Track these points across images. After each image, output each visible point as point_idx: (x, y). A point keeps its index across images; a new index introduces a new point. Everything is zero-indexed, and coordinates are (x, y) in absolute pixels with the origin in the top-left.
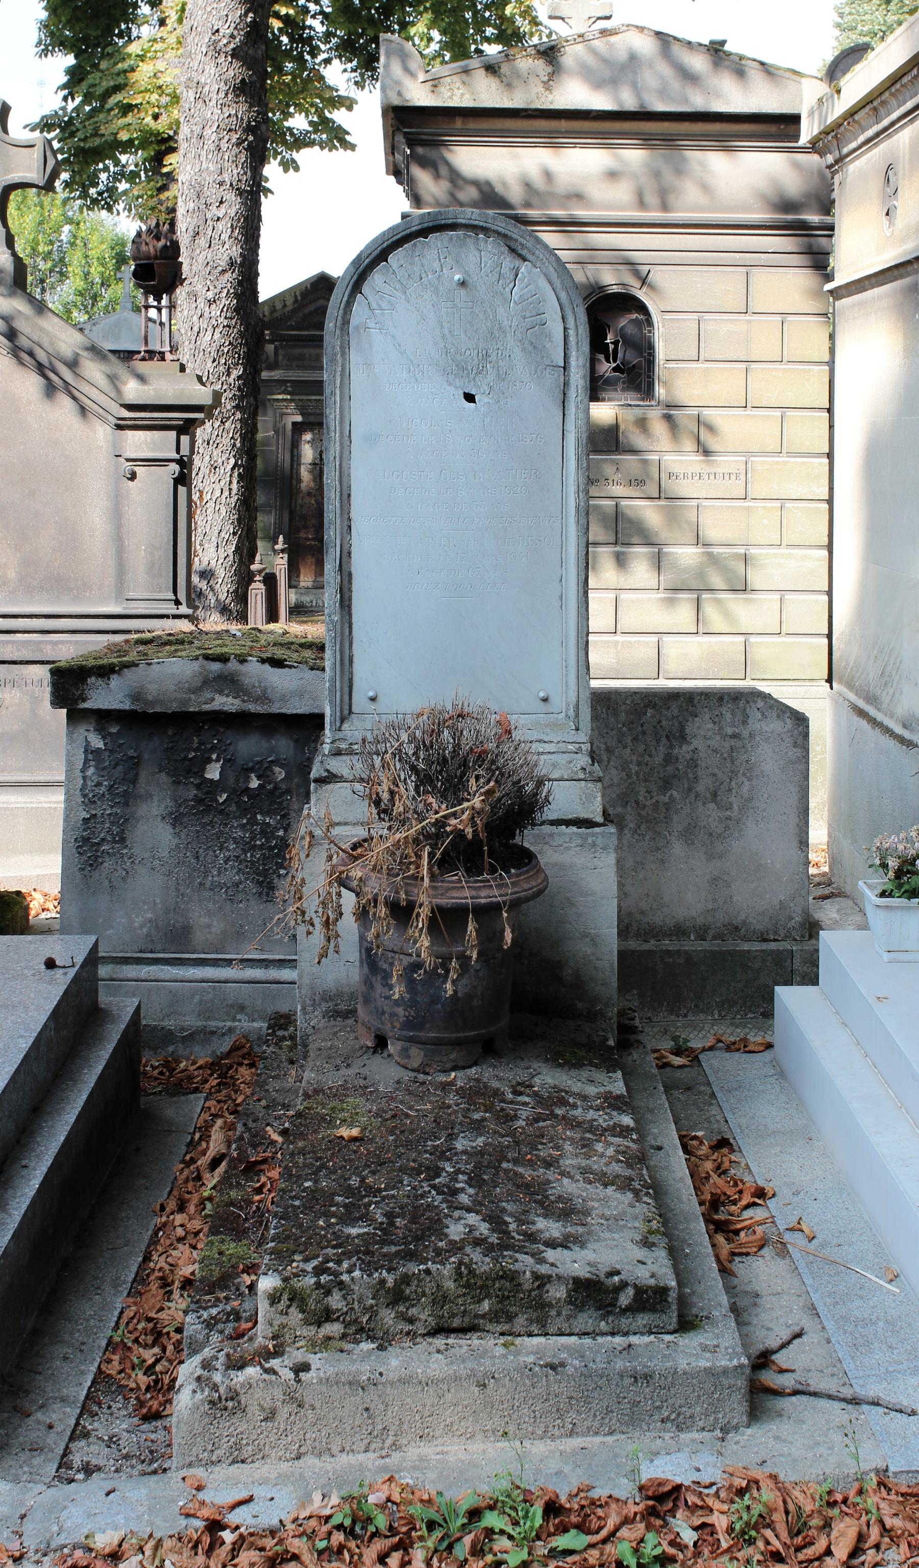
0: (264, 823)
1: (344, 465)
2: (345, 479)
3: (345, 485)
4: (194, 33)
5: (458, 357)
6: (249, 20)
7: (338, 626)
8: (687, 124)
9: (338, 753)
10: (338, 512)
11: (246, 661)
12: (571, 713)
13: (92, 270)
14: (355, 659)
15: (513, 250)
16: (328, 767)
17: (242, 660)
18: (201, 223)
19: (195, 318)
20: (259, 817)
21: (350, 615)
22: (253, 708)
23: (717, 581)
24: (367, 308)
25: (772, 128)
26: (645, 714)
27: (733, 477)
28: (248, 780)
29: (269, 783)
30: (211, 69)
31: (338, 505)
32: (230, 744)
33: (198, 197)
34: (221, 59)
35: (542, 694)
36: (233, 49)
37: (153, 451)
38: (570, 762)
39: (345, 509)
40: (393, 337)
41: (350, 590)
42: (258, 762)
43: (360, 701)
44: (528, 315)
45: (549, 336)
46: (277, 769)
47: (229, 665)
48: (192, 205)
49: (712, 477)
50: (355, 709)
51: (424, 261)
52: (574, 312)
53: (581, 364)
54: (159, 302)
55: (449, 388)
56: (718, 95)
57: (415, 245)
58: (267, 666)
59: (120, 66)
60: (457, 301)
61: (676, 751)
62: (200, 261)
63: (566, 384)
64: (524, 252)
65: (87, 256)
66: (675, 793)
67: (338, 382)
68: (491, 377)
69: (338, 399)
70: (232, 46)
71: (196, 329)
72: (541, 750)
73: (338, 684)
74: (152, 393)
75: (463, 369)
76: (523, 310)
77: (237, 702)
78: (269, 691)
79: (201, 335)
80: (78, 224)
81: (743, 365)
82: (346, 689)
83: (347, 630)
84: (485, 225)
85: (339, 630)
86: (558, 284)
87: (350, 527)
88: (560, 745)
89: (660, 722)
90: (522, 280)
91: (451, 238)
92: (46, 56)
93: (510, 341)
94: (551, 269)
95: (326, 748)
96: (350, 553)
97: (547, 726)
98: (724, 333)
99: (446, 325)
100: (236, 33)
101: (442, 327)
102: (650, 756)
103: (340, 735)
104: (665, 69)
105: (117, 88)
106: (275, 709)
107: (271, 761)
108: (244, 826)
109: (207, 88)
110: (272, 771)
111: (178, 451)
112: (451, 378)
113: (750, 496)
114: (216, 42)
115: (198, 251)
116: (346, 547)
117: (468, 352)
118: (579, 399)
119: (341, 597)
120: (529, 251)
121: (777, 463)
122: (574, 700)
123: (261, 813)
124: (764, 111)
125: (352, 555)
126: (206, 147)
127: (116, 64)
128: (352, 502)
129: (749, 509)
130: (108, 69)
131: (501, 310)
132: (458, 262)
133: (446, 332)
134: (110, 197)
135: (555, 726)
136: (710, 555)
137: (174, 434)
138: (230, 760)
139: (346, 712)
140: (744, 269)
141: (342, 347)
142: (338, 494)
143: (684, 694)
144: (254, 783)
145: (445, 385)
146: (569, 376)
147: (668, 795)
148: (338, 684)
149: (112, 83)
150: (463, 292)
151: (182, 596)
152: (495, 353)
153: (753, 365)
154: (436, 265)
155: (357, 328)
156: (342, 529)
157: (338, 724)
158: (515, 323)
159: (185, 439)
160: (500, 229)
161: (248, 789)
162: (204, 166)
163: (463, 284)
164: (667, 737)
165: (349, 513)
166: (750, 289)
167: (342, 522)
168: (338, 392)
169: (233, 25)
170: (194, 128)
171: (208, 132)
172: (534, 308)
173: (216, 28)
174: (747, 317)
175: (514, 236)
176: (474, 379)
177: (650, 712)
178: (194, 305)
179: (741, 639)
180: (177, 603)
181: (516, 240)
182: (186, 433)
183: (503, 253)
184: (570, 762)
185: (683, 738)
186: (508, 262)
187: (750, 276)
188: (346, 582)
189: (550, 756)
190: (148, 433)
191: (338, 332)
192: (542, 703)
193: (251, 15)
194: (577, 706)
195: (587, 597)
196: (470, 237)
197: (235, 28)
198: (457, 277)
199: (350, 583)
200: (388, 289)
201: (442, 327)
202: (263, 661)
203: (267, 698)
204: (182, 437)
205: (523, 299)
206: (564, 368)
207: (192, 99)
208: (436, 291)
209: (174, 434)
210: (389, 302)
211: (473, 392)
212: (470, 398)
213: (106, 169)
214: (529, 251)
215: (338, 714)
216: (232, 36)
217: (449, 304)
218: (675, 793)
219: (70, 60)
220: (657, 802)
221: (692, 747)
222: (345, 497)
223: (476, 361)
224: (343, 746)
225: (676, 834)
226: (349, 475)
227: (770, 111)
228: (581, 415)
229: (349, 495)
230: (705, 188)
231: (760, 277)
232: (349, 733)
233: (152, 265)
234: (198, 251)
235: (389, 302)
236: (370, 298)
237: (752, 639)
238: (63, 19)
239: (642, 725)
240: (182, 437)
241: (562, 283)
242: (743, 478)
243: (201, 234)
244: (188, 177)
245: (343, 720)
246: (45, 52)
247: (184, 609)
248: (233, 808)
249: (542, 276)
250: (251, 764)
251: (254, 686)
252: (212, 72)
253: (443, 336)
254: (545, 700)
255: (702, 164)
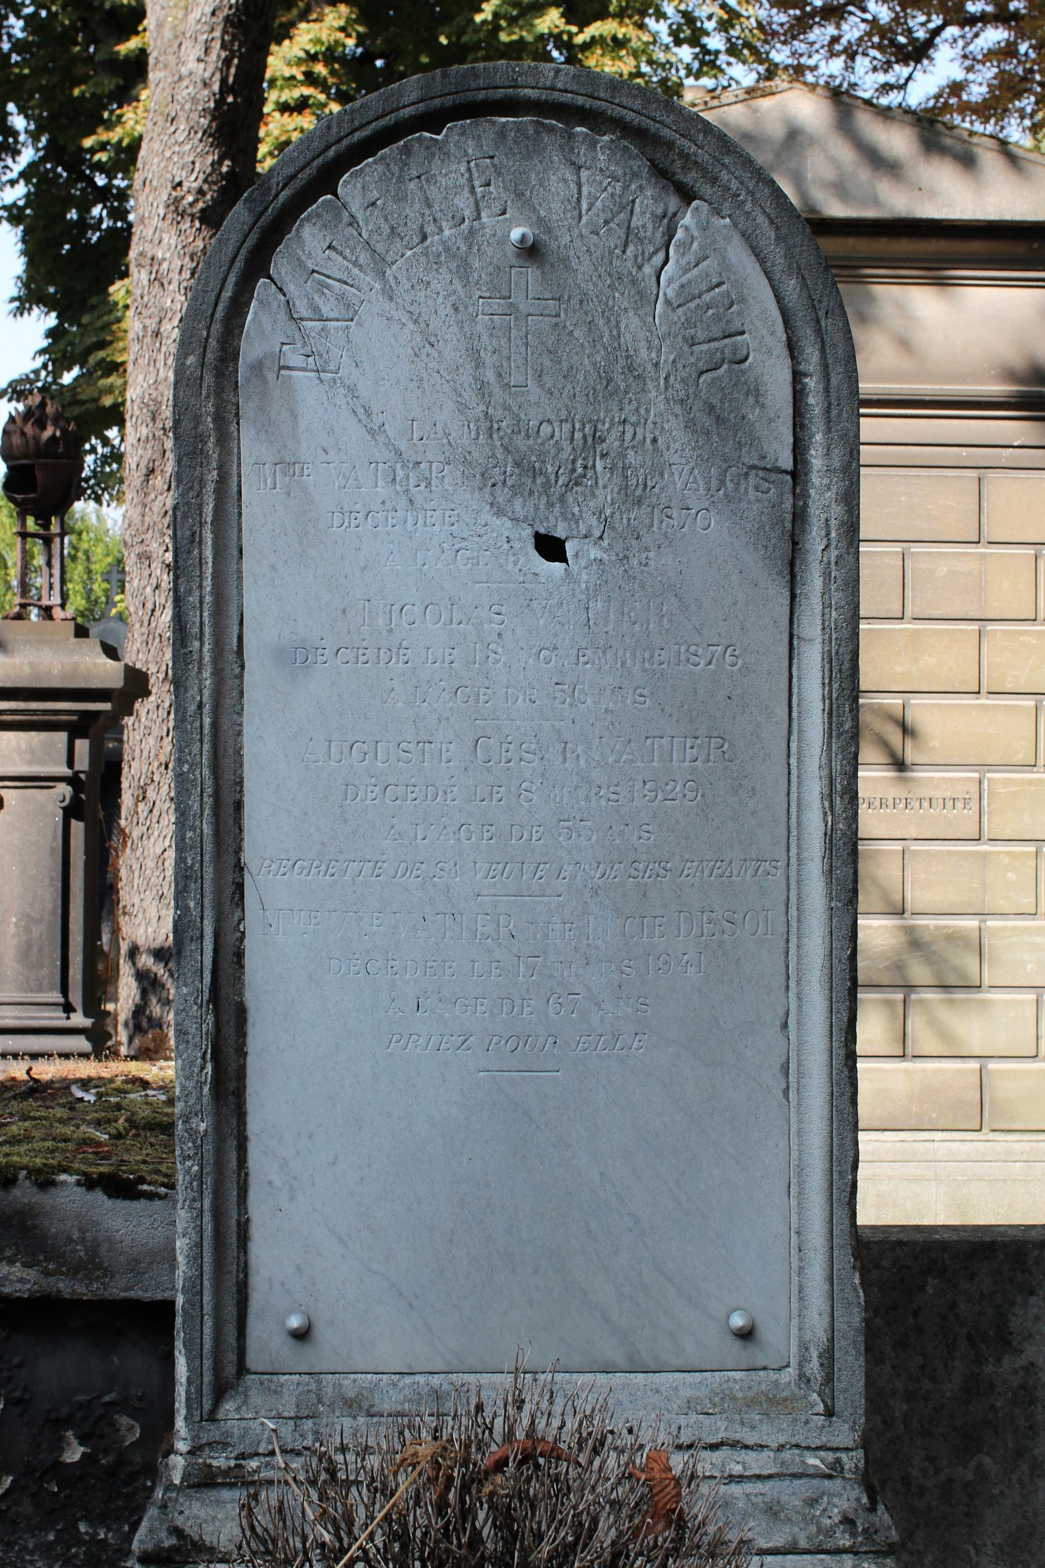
0: (94, 1540)
1: (225, 725)
2: (227, 762)
3: (228, 776)
4: (147, 189)
5: (519, 441)
6: (224, 169)
7: (208, 1147)
8: (884, 240)
9: (204, 1481)
10: (208, 847)
11: (53, 1183)
12: (814, 1366)
13: (96, 587)
14: (256, 1232)
15: (661, 173)
16: (179, 1521)
17: (44, 1180)
18: (157, 455)
19: (149, 590)
20: (83, 1528)
21: (241, 1116)
22: (65, 1287)
23: (919, 973)
24: (283, 316)
25: (1019, 248)
26: (922, 1288)
27: (959, 805)
28: (59, 1445)
29: (106, 1452)
30: (170, 238)
31: (207, 829)
32: (21, 1365)
33: (154, 419)
34: (186, 225)
35: (738, 1321)
36: (202, 211)
37: (30, 762)
38: (813, 1502)
39: (229, 840)
40: (352, 390)
41: (242, 1053)
42: (81, 1406)
43: (266, 1341)
44: (701, 335)
45: (756, 392)
46: (124, 1421)
47: (16, 1192)
48: (144, 431)
49: (926, 804)
50: (253, 1360)
51: (433, 192)
52: (819, 331)
53: (836, 464)
54: (46, 526)
55: (496, 522)
56: (932, 195)
57: (407, 150)
58: (99, 1197)
59: (105, 318)
60: (518, 297)
61: (989, 1369)
62: (155, 509)
63: (799, 517)
64: (690, 178)
65: (90, 571)
66: (987, 1461)
67: (209, 510)
68: (606, 495)
69: (208, 553)
70: (201, 205)
71: (149, 606)
72: (738, 1469)
73: (207, 1298)
74: (27, 670)
75: (535, 473)
76: (689, 324)
77: (31, 1274)
78: (103, 1250)
79: (157, 613)
80: (80, 534)
81: (974, 627)
82: (230, 1311)
83: (233, 1157)
84: (588, 103)
85: (209, 1156)
86: (778, 258)
87: (240, 887)
88: (787, 1455)
89: (953, 1305)
90: (685, 246)
91: (502, 133)
92: (22, 314)
93: (656, 401)
94: (761, 219)
95: (177, 1466)
96: (240, 955)
97: (751, 1403)
98: (943, 572)
99: (488, 359)
100: (206, 187)
101: (478, 364)
102: (933, 1379)
103: (213, 1432)
104: (844, 152)
105: (102, 345)
106: (117, 1290)
107: (112, 1403)
108: (51, 1546)
109: (165, 266)
110: (112, 1424)
111: (70, 763)
112: (502, 495)
113: (986, 834)
114: (177, 201)
115: (153, 496)
116: (231, 938)
117: (546, 430)
118: (834, 554)
119: (216, 1070)
120: (704, 171)
121: (1030, 782)
122: (822, 1336)
123: (88, 1518)
124: (1008, 217)
125: (249, 962)
126: (164, 349)
127: (100, 317)
128: (248, 823)
129: (985, 855)
130: (91, 323)
131: (631, 323)
132: (519, 195)
133: (490, 376)
134: (98, 484)
135: (772, 1404)
136: (909, 930)
137: (62, 737)
138: (19, 1401)
139: (230, 1370)
140: (974, 473)
141: (219, 419)
142: (208, 801)
143: (1005, 1244)
144: (74, 1453)
145: (486, 515)
146: (805, 496)
147: (973, 1464)
148: (207, 1298)
149: (94, 339)
150: (532, 273)
151: (76, 998)
152: (615, 433)
153: (991, 627)
154: (463, 203)
155: (258, 367)
156: (218, 893)
157: (207, 1405)
158: (667, 356)
159: (82, 746)
160: (630, 116)
161: (58, 1466)
162: (162, 375)
163: (531, 251)
164: (970, 1339)
165: (238, 850)
166: (985, 504)
167: (218, 874)
168: (208, 536)
169: (202, 176)
170: (148, 322)
171: (166, 327)
172: (717, 318)
173: (177, 180)
174: (980, 550)
175: (666, 133)
176: (562, 500)
177: (932, 1285)
178: (147, 572)
179: (974, 1065)
180: (68, 1008)
181: (670, 145)
182: (83, 735)
183: (635, 175)
184: (813, 1502)
185: (1004, 1341)
186: (649, 202)
187: (984, 484)
188: (229, 1031)
189: (759, 1487)
190: (22, 735)
191: (209, 379)
192: (738, 1343)
193: (227, 163)
194: (828, 1356)
195: (853, 1070)
196: (551, 130)
197: (205, 181)
198: (516, 234)
199: (241, 1033)
200: (337, 265)
201: (478, 364)
202: (89, 1183)
203: (99, 1267)
204: (78, 743)
205: (686, 295)
206: (794, 474)
207: (146, 283)
208: (464, 270)
209: (62, 737)
210: (341, 297)
211: (560, 533)
212: (551, 548)
213: (93, 450)
214: (704, 171)
215: (207, 1378)
216: (201, 192)
217: (496, 305)
218: (987, 1461)
219: (52, 320)
220: (950, 1480)
221: (1022, 1361)
222: (228, 810)
223: (566, 453)
224: (221, 1461)
225: (990, 1550)
226: (238, 753)
227: (1018, 218)
228: (837, 597)
229: (239, 806)
230: (905, 344)
231: (999, 484)
232: (234, 1427)
233: (31, 468)
234: (153, 496)
235: (341, 297)
236: (291, 288)
237: (992, 1065)
238: (42, 270)
239: (915, 1314)
240: (78, 743)
241: (789, 255)
242: (975, 806)
243: (158, 472)
244: (139, 391)
245: (221, 1391)
246: (20, 311)
247: (78, 1019)
248: (27, 1507)
249: (737, 240)
250: (65, 1411)
251: (70, 1240)
252: (173, 242)
253: (482, 389)
254: (746, 1335)
255: (901, 307)
